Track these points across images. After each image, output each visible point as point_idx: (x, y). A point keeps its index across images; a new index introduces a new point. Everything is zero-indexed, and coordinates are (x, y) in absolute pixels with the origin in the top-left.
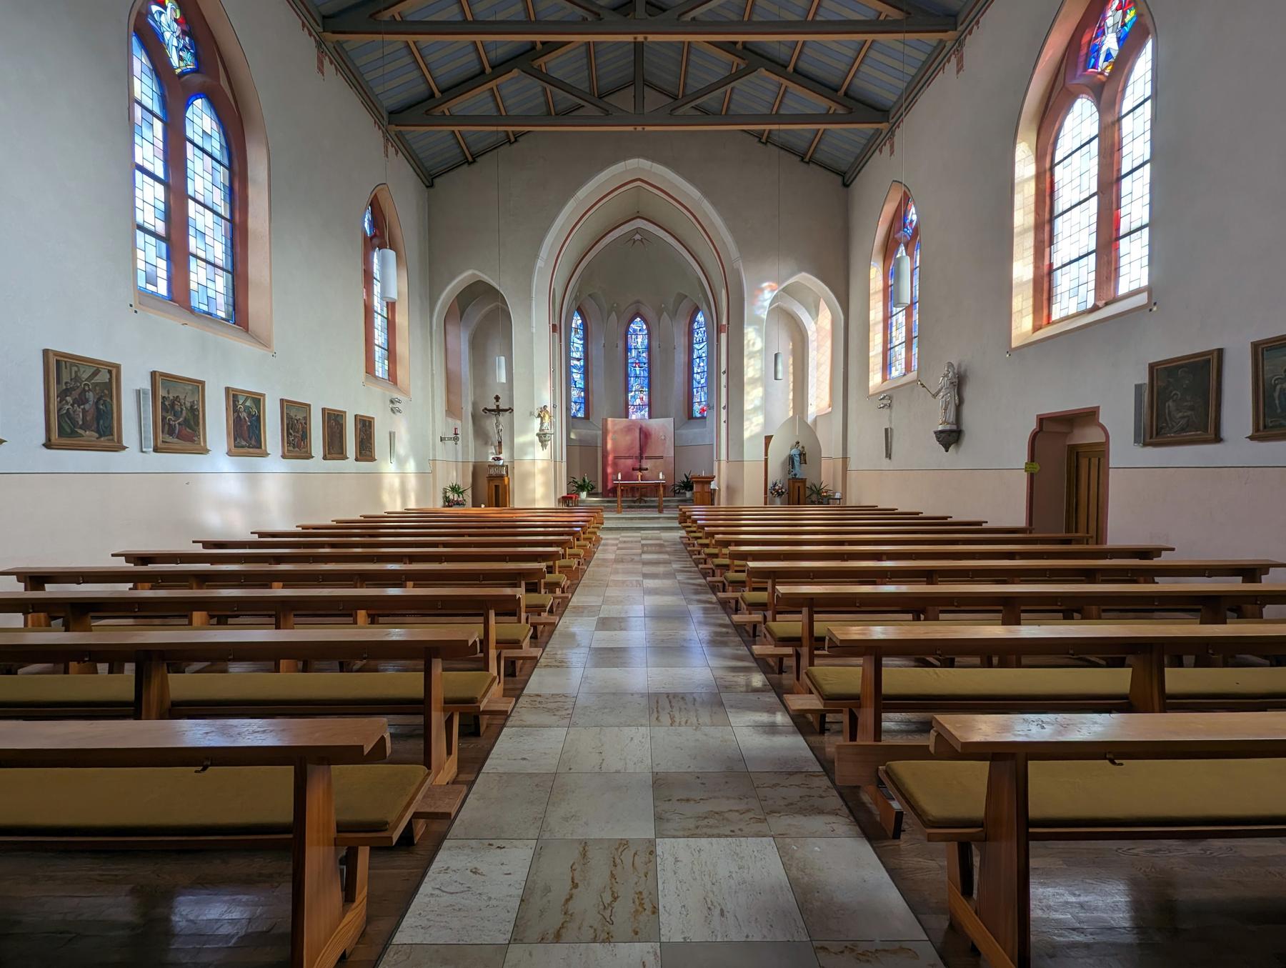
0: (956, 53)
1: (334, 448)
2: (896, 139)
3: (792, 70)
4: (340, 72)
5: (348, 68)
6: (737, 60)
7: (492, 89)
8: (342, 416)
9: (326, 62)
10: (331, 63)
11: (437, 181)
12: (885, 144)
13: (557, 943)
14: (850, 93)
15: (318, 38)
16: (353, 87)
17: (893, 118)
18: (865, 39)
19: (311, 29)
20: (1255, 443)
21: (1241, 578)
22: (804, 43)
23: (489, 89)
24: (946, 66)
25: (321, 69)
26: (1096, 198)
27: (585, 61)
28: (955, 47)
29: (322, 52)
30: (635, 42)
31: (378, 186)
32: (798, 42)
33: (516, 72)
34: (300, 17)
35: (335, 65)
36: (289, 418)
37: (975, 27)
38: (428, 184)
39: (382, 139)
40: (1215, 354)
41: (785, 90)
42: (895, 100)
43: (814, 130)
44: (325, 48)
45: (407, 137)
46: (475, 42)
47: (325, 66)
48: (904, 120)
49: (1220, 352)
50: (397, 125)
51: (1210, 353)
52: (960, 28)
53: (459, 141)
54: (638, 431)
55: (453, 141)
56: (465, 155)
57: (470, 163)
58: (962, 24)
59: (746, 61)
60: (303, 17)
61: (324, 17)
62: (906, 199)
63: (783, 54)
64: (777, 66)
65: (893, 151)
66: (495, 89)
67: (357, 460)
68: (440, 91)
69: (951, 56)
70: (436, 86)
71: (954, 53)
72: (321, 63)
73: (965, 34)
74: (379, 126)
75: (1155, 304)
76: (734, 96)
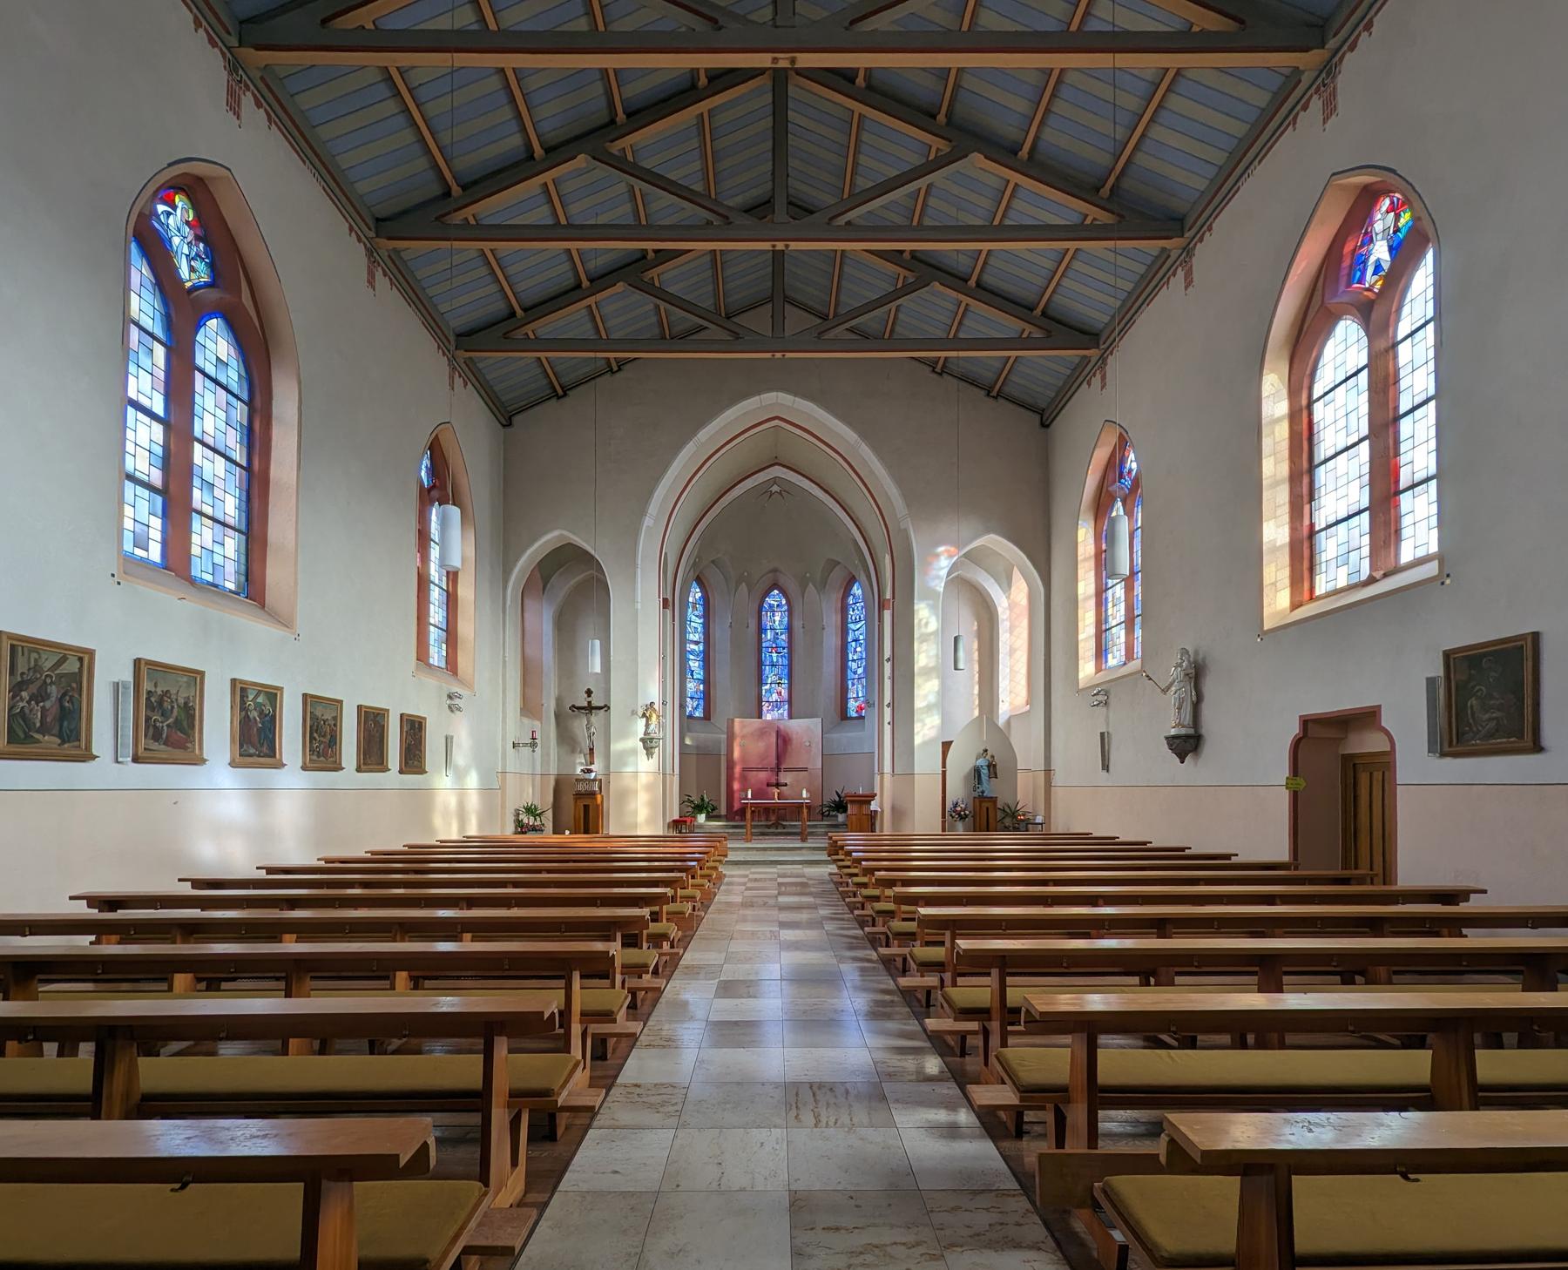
0: (1322, 88)
6: (903, 272)
8: (276, 694)
10: (385, 274)
25: (371, 282)
29: (240, 82)
33: (582, 160)
36: (314, 717)
38: (505, 423)
48: (1214, 225)
49: (1536, 636)
51: (1522, 637)
55: (539, 370)
57: (559, 398)
60: (195, 10)
64: (956, 279)
73: (1167, 276)
75: (1448, 576)
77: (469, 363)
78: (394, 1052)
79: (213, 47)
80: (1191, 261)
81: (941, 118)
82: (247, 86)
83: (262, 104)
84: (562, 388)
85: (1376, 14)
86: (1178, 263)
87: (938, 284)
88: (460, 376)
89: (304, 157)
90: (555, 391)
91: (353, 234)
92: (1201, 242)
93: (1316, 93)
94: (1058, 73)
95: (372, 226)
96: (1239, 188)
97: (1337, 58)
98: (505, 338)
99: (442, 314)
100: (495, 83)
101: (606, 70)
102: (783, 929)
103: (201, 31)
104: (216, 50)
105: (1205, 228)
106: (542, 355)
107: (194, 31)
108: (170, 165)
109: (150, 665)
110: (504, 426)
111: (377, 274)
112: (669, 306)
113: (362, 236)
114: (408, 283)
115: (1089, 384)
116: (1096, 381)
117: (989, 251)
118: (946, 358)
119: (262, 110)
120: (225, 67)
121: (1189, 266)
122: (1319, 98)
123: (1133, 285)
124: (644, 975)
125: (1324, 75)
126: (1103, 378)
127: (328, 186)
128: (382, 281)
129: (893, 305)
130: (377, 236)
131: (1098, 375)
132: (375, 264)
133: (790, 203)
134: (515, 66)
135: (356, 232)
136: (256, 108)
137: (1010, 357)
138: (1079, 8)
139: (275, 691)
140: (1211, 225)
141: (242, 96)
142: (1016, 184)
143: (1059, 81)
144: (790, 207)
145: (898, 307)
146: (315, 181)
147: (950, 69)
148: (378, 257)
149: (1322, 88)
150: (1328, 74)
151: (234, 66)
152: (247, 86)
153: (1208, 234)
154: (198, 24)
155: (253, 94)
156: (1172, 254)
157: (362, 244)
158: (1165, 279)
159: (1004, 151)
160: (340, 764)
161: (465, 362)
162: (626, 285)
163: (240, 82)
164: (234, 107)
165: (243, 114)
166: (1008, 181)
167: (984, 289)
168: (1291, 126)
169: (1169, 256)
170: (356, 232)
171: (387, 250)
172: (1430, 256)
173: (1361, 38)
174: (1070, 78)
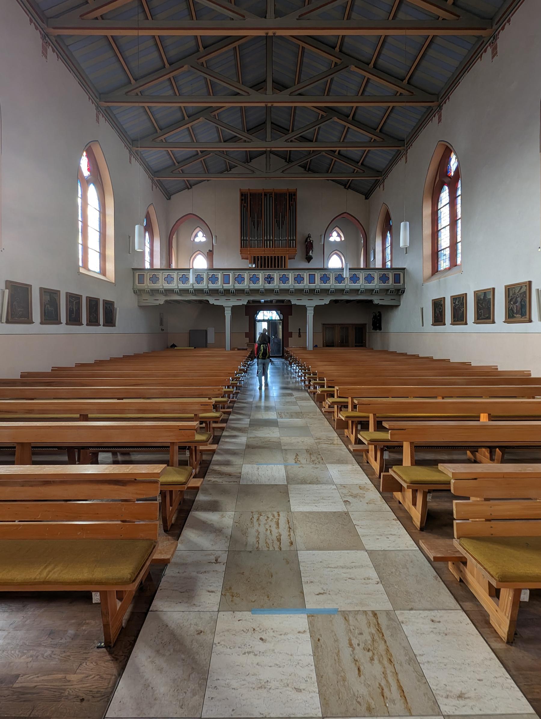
0: (492, 44)
1: (93, 321)
2: (499, 42)
3: (351, 119)
4: (108, 121)
5: (114, 122)
6: (335, 60)
7: (188, 128)
8: (80, 298)
9: (50, 50)
10: (54, 51)
11: (172, 197)
12: (434, 116)
13: (222, 594)
14: (365, 163)
15: (96, 104)
16: (114, 129)
17: (441, 99)
18: (389, 105)
19: (93, 100)
20: (475, 324)
21: (289, 338)
22: (357, 107)
23: (187, 128)
24: (483, 55)
25: (98, 121)
26: (449, 226)
27: (239, 114)
28: (491, 40)
29: (47, 43)
30: (266, 36)
31: (92, 141)
32: (353, 107)
33: (201, 119)
34: (28, 15)
35: (56, 53)
36: (106, 308)
37: (448, 100)
38: (168, 198)
39: (129, 154)
40: (492, 290)
41: (368, 81)
42: (415, 125)
43: (362, 150)
44: (100, 109)
45: (115, 112)
46: (181, 107)
47: (48, 53)
48: (511, 19)
49: (466, 294)
50: (157, 177)
51: (441, 298)
52: (495, 27)
53: (171, 157)
54: (276, 19)
55: (168, 157)
56: (187, 185)
57: (189, 189)
58: (383, 175)
59: (327, 114)
60: (30, 15)
61: (133, 141)
62: (447, 152)
63: (367, 51)
64: (344, 116)
65: (407, 161)
66: (190, 128)
67: (42, 323)
68: (134, 79)
69: (487, 47)
70: (158, 126)
71: (490, 44)
72: (97, 117)
73: (432, 117)
74: (127, 147)
75: (539, 248)
76: (333, 87)
77: (159, 181)
78: (78, 464)
79: (36, 30)
80: (441, 111)
81: (337, 49)
82: (49, 44)
83: (55, 51)
84: (190, 186)
85: (450, 95)
86: (488, 44)
87: (354, 66)
88: (134, 157)
89: (113, 127)
90: (187, 186)
91: (90, 100)
92: (435, 117)
93: (507, 22)
94: (384, 37)
95: (98, 96)
96: (460, 82)
97: (497, 33)
98: (127, 95)
99: (67, 46)
100: (151, 43)
101: (197, 36)
102: (276, 419)
103: (32, 24)
104: (38, 31)
105: (447, 98)
106: (169, 149)
107: (57, 60)
108: (86, 146)
109: (12, 283)
110: (167, 199)
111: (100, 116)
112: (212, 79)
113: (94, 101)
114: (81, 76)
115: (379, 187)
116: (436, 119)
117: (357, 107)
118: (386, 36)
119: (38, 31)
120: (41, 38)
121: (440, 113)
122: (491, 48)
123: (416, 124)
124: (215, 410)
125: (492, 39)
126: (406, 159)
127: (81, 81)
128: (102, 119)
129: (329, 78)
130: (100, 101)
131: (437, 116)
132: (47, 44)
133: (272, 123)
134: (159, 35)
135: (91, 100)
136: (35, 30)
137: (389, 107)
138: (391, 14)
139: (28, 287)
140: (510, 19)
141: (48, 49)
142: (368, 78)
143: (384, 41)
144: (272, 125)
145: (319, 128)
146: (71, 74)
147: (339, 36)
148: (48, 40)
149: (492, 44)
150: (494, 38)
151: (98, 107)
152: (49, 44)
153: (507, 24)
154: (31, 21)
155: (52, 47)
156: (402, 151)
157: (55, 53)
158: (480, 55)
159: (363, 64)
160: (32, 320)
161: (136, 152)
162: (204, 119)
163: (47, 43)
164: (45, 53)
165: (48, 57)
166: (365, 77)
167: (341, 155)
168: (480, 59)
169: (433, 109)
170: (91, 100)
171: (55, 36)
172: (389, 235)
173: (506, 26)
174: (389, 40)
